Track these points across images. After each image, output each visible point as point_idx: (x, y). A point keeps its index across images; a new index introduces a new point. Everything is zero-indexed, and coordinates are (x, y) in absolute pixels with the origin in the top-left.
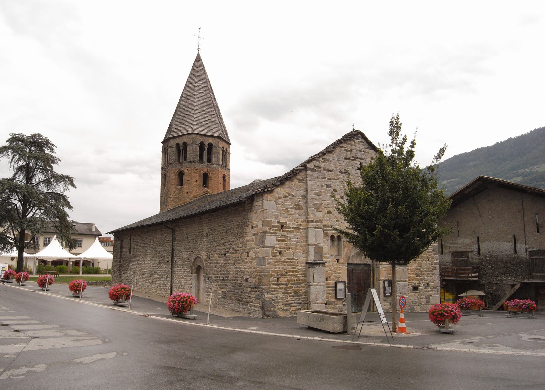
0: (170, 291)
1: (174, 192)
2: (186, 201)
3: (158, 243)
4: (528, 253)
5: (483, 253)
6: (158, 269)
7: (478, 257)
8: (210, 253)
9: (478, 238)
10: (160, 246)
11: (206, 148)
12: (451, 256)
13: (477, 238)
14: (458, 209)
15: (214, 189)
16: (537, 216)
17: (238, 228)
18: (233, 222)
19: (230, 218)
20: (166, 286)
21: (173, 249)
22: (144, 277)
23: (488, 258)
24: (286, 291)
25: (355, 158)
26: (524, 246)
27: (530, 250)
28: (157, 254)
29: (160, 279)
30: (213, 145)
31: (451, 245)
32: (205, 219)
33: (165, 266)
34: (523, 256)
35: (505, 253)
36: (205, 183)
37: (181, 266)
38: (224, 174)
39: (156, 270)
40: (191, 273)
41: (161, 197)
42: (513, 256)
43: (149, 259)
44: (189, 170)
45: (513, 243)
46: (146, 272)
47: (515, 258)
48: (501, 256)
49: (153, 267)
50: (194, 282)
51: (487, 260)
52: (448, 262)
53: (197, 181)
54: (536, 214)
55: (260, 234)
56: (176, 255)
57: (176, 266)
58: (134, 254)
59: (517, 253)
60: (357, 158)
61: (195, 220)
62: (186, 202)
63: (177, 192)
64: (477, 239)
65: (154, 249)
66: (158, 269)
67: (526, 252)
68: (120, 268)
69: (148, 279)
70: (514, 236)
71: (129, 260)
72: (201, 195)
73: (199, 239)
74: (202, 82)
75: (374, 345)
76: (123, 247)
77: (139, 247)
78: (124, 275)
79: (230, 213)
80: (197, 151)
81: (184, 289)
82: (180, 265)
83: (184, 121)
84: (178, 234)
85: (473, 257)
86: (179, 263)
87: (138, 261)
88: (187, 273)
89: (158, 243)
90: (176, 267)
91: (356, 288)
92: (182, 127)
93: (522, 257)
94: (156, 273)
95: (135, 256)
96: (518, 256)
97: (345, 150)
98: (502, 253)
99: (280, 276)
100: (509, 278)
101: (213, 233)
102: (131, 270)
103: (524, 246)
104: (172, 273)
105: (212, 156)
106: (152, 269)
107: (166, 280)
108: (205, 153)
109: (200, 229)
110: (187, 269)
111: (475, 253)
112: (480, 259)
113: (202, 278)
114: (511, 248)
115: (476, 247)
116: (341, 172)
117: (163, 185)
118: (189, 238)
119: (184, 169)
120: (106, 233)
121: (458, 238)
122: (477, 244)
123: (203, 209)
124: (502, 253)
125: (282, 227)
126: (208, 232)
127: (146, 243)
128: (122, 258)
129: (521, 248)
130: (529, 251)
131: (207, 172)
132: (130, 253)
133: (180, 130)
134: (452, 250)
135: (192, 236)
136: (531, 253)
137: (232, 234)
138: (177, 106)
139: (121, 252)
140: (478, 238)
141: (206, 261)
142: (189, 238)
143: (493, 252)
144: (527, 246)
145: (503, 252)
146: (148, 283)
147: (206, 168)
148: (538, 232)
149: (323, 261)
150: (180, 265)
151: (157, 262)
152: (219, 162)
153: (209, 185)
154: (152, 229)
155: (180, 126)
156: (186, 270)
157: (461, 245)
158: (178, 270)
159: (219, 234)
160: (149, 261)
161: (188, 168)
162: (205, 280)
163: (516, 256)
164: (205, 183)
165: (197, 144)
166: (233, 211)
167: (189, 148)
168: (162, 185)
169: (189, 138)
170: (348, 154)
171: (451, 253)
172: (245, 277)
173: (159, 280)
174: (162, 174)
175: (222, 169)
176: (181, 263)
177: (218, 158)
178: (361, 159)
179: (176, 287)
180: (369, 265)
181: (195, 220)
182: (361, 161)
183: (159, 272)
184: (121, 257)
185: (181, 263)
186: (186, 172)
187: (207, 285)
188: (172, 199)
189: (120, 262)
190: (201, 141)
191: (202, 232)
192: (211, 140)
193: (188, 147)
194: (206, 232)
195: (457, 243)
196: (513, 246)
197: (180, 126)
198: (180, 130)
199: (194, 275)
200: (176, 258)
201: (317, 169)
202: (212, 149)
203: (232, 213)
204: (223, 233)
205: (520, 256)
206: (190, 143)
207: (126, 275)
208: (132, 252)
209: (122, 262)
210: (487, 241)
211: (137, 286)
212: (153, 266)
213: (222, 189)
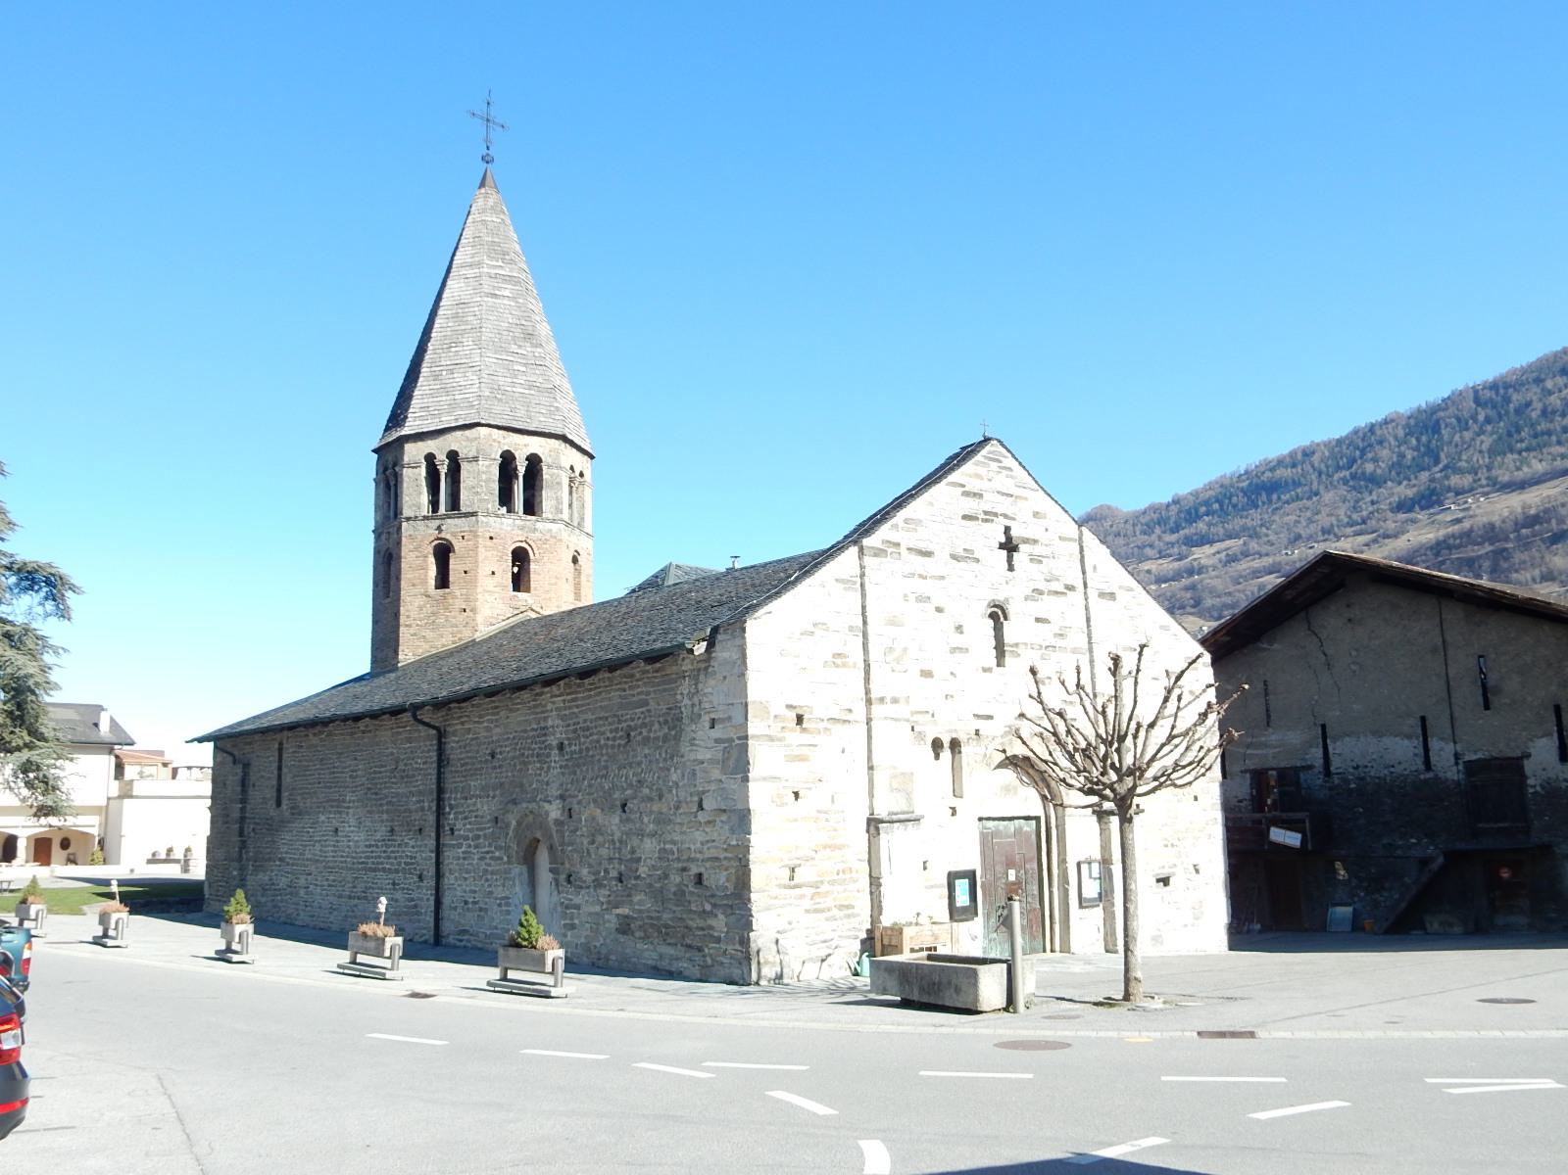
0: (432, 920)
1: (421, 608)
2: (459, 636)
3: (386, 772)
4: (1461, 767)
5: (1339, 771)
6: (385, 852)
7: (1326, 782)
8: (575, 801)
9: (1323, 727)
10: (393, 780)
11: (521, 470)
12: (1249, 782)
13: (1320, 728)
14: (1265, 646)
15: (548, 596)
16: (1482, 660)
17: (666, 722)
18: (648, 708)
19: (638, 694)
20: (416, 906)
21: (440, 791)
22: (334, 881)
23: (1353, 786)
24: (815, 904)
25: (990, 516)
26: (1450, 748)
27: (1467, 758)
28: (381, 805)
29: (394, 884)
30: (540, 461)
31: (1249, 752)
32: (552, 697)
33: (412, 843)
34: (1449, 775)
35: (1398, 769)
36: (520, 582)
37: (472, 843)
38: (576, 551)
39: (380, 857)
40: (509, 862)
41: (375, 622)
42: (1422, 777)
43: (352, 821)
44: (468, 540)
45: (1421, 739)
46: (342, 862)
47: (1426, 781)
48: (1388, 779)
49: (366, 846)
50: (517, 889)
51: (1351, 791)
52: (1240, 801)
53: (493, 573)
54: (1480, 657)
55: (737, 742)
56: (451, 808)
57: (454, 842)
58: (292, 808)
59: (1433, 768)
60: (996, 515)
61: (519, 701)
62: (460, 639)
63: (428, 609)
64: (1320, 732)
65: (369, 789)
66: (385, 852)
67: (1457, 764)
68: (240, 852)
69: (351, 885)
70: (1423, 719)
71: (273, 827)
72: (508, 618)
73: (532, 757)
74: (500, 263)
75: (1077, 1030)
76: (251, 783)
77: (314, 783)
78: (256, 875)
79: (637, 680)
80: (494, 481)
81: (482, 913)
82: (466, 838)
83: (449, 386)
84: (458, 742)
85: (1314, 780)
86: (462, 832)
87: (311, 830)
88: (493, 862)
89: (386, 772)
90: (453, 846)
91: (1003, 886)
92: (442, 403)
93: (1447, 780)
94: (380, 866)
95: (297, 812)
96: (1437, 778)
97: (964, 486)
98: (1392, 769)
99: (798, 862)
100: (1414, 841)
101: (582, 740)
102: (281, 860)
103: (1450, 748)
104: (438, 863)
105: (541, 496)
106: (364, 852)
107: (419, 887)
108: (519, 488)
109: (535, 727)
110: (493, 849)
111: (1316, 771)
112: (1330, 789)
113: (545, 876)
114: (1416, 755)
115: (1318, 753)
116: (954, 557)
117: (381, 585)
118: (498, 756)
119: (454, 534)
120: (187, 742)
121: (1266, 730)
122: (1321, 745)
123: (601, 677)
124: (1392, 769)
125: (800, 719)
126: (564, 736)
127: (338, 773)
128: (248, 821)
129: (1443, 753)
130: (1464, 762)
131: (524, 545)
132: (279, 804)
133: (436, 412)
134: (1251, 764)
135: (507, 749)
136: (1471, 768)
137: (646, 741)
138: (420, 335)
139: (243, 801)
140: (1323, 727)
141: (559, 823)
142: (498, 756)
143: (1366, 767)
144: (1459, 749)
145: (1393, 766)
146: (350, 897)
147: (520, 532)
148: (1487, 707)
149: (913, 812)
150: (466, 838)
151: (382, 832)
152: (561, 513)
153: (533, 584)
154: (362, 728)
155: (438, 399)
156: (488, 852)
157: (1277, 750)
158: (461, 855)
159: (602, 742)
160: (352, 828)
161: (464, 532)
162: (557, 881)
163: (1430, 775)
164: (520, 582)
165: (493, 456)
166: (650, 675)
167: (468, 471)
168: (376, 584)
169: (468, 439)
170: (972, 506)
171: (1248, 775)
172: (694, 870)
173: (391, 886)
174: (377, 552)
175: (569, 536)
176: (470, 830)
177: (559, 501)
178: (1006, 516)
179: (455, 908)
180: (1037, 819)
181: (519, 701)
182: (1008, 523)
183: (392, 864)
184: (242, 819)
185: (470, 830)
186: (457, 544)
187: (563, 898)
188: (412, 631)
189: (241, 833)
190: (506, 448)
191: (545, 735)
192: (536, 445)
193: (465, 467)
194: (558, 736)
195: (1265, 745)
196: (1420, 750)
197: (438, 399)
198: (436, 412)
199: (518, 870)
200: (452, 816)
201: (890, 550)
202: (536, 475)
203: (645, 680)
204: (614, 739)
205: (1441, 775)
206: (471, 455)
207: (264, 877)
208: (285, 802)
209: (249, 833)
210: (1348, 735)
211: (309, 908)
212: (368, 843)
213: (572, 597)
